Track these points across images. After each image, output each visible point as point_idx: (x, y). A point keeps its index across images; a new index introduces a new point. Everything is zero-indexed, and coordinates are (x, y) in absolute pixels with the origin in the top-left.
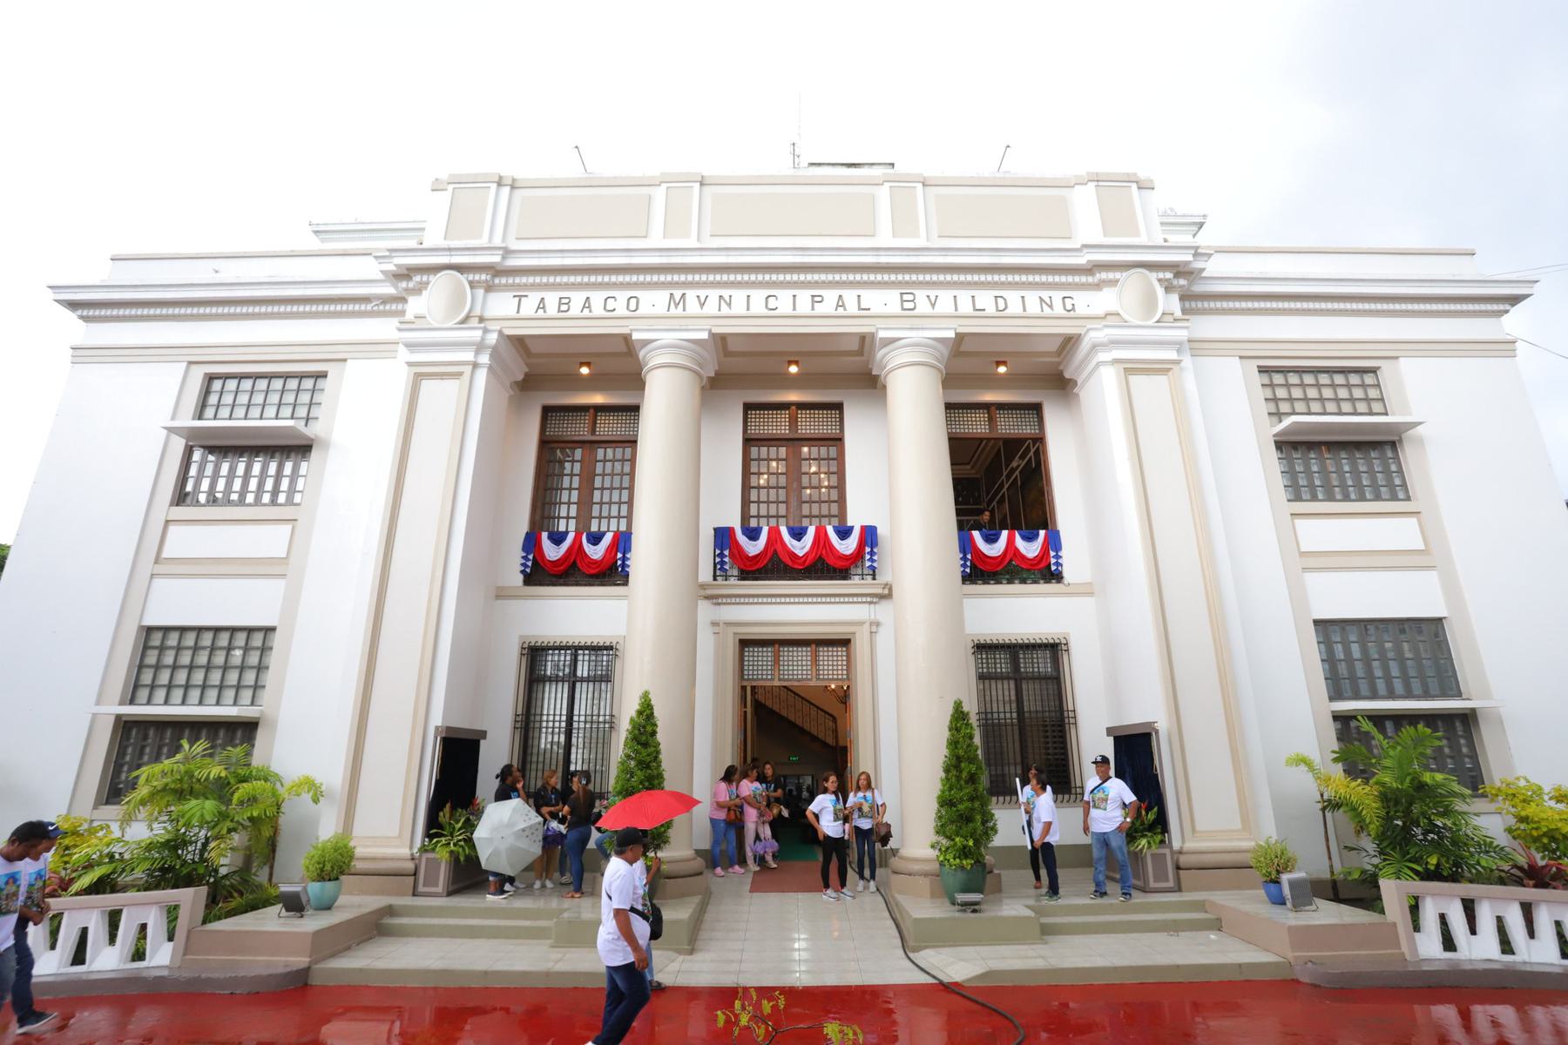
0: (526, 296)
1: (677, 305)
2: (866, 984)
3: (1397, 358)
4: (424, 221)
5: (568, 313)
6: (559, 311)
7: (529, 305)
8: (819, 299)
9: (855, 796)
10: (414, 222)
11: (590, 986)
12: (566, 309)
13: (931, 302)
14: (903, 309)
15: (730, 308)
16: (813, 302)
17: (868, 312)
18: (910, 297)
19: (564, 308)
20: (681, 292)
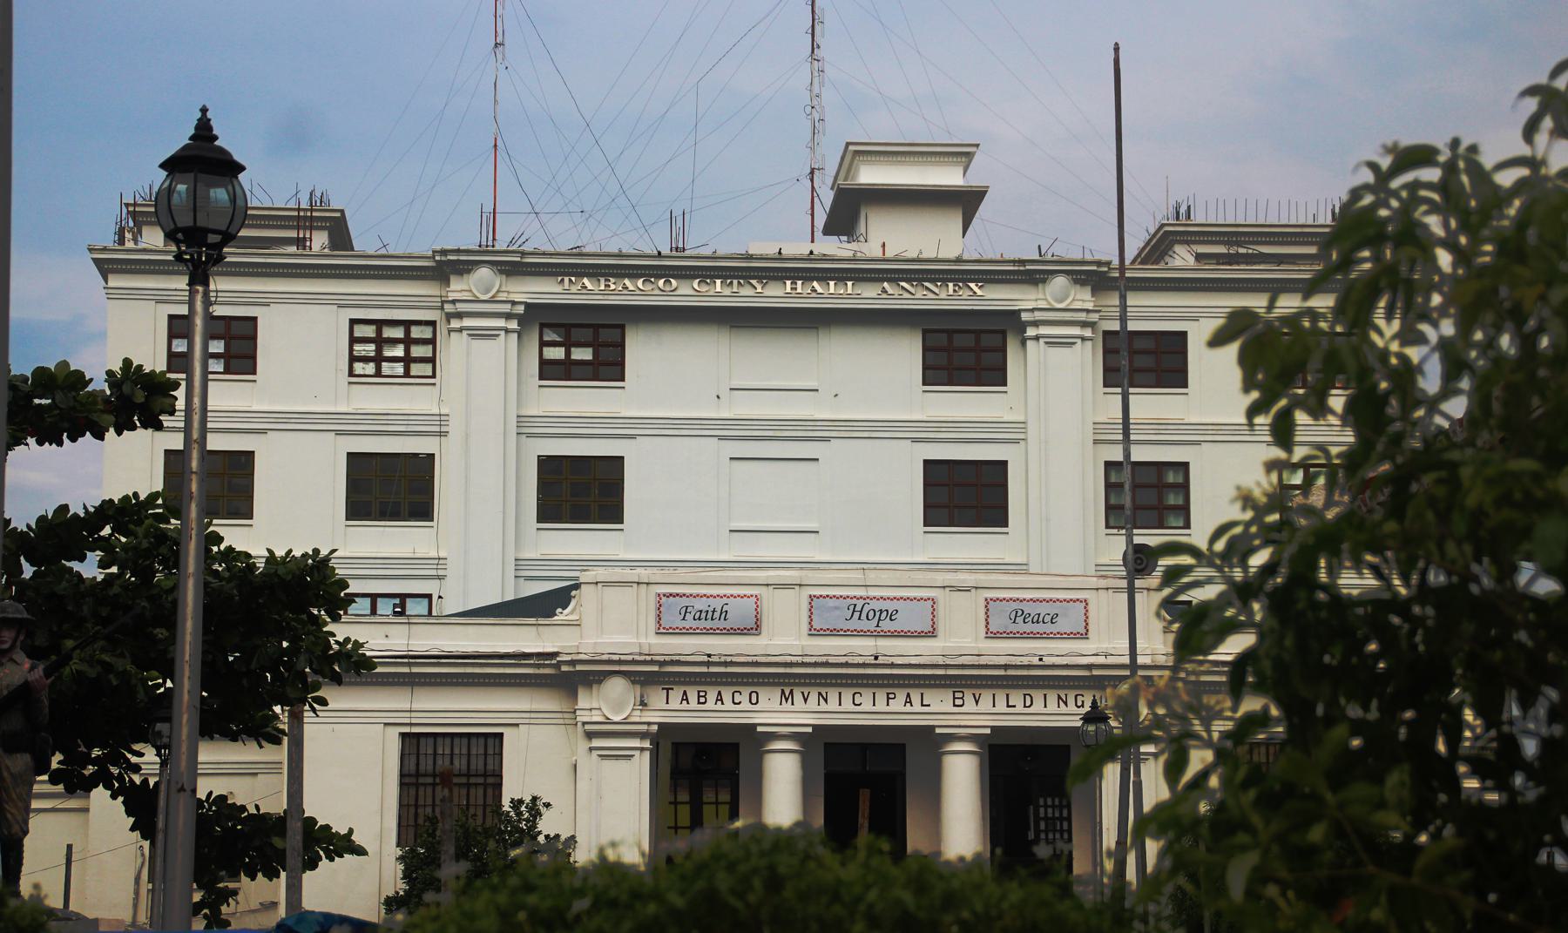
0: (672, 689)
1: (787, 700)
2: (1036, 743)
3: (256, 774)
4: (448, 415)
5: (963, 708)
6: (699, 703)
7: (898, 704)
8: (892, 696)
9: (442, 791)
10: (176, 290)
11: (30, 826)
12: (961, 703)
13: (804, 696)
14: (955, 705)
15: (1067, 706)
16: (888, 698)
17: (1013, 709)
18: (960, 695)
19: (702, 700)
20: (790, 688)
